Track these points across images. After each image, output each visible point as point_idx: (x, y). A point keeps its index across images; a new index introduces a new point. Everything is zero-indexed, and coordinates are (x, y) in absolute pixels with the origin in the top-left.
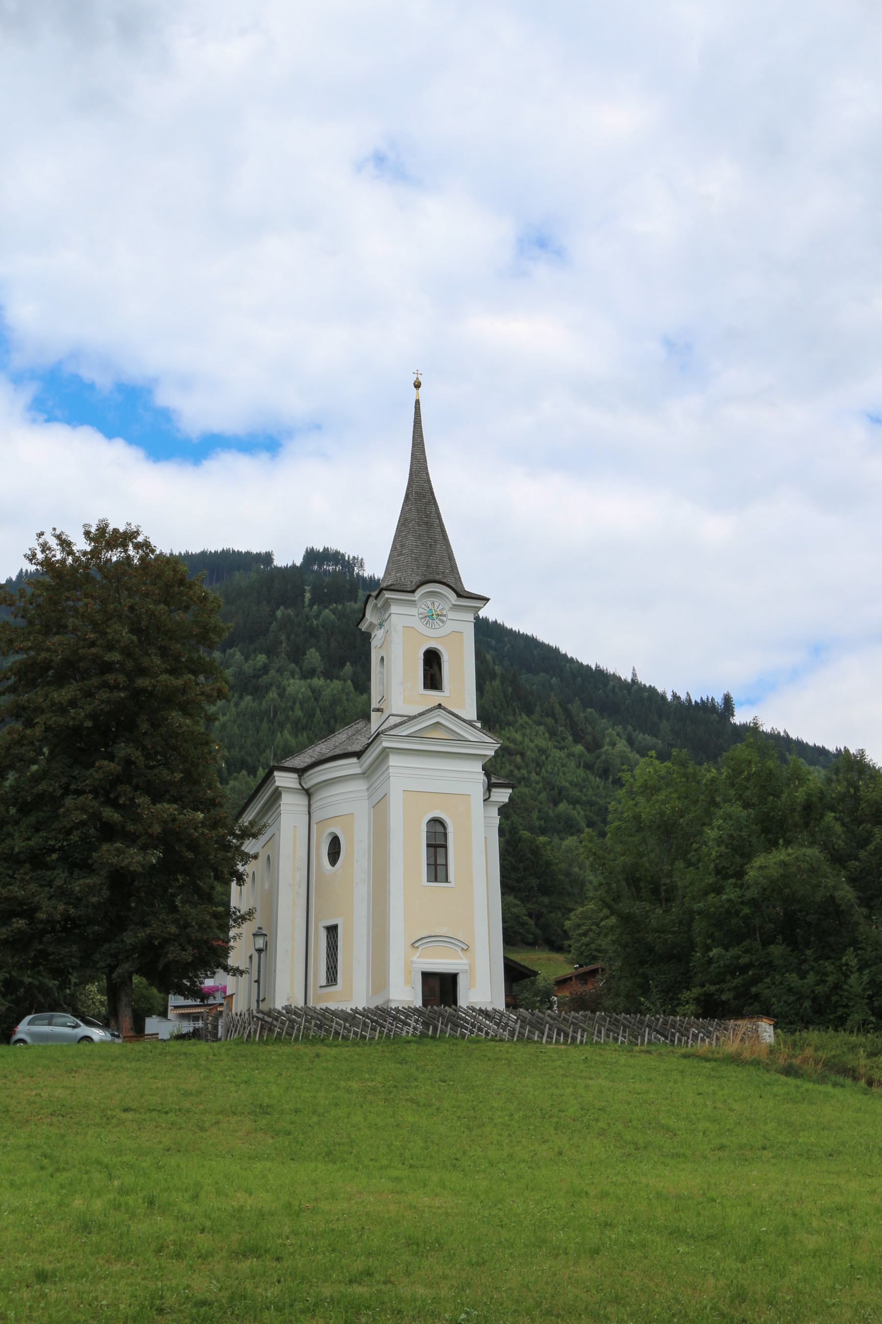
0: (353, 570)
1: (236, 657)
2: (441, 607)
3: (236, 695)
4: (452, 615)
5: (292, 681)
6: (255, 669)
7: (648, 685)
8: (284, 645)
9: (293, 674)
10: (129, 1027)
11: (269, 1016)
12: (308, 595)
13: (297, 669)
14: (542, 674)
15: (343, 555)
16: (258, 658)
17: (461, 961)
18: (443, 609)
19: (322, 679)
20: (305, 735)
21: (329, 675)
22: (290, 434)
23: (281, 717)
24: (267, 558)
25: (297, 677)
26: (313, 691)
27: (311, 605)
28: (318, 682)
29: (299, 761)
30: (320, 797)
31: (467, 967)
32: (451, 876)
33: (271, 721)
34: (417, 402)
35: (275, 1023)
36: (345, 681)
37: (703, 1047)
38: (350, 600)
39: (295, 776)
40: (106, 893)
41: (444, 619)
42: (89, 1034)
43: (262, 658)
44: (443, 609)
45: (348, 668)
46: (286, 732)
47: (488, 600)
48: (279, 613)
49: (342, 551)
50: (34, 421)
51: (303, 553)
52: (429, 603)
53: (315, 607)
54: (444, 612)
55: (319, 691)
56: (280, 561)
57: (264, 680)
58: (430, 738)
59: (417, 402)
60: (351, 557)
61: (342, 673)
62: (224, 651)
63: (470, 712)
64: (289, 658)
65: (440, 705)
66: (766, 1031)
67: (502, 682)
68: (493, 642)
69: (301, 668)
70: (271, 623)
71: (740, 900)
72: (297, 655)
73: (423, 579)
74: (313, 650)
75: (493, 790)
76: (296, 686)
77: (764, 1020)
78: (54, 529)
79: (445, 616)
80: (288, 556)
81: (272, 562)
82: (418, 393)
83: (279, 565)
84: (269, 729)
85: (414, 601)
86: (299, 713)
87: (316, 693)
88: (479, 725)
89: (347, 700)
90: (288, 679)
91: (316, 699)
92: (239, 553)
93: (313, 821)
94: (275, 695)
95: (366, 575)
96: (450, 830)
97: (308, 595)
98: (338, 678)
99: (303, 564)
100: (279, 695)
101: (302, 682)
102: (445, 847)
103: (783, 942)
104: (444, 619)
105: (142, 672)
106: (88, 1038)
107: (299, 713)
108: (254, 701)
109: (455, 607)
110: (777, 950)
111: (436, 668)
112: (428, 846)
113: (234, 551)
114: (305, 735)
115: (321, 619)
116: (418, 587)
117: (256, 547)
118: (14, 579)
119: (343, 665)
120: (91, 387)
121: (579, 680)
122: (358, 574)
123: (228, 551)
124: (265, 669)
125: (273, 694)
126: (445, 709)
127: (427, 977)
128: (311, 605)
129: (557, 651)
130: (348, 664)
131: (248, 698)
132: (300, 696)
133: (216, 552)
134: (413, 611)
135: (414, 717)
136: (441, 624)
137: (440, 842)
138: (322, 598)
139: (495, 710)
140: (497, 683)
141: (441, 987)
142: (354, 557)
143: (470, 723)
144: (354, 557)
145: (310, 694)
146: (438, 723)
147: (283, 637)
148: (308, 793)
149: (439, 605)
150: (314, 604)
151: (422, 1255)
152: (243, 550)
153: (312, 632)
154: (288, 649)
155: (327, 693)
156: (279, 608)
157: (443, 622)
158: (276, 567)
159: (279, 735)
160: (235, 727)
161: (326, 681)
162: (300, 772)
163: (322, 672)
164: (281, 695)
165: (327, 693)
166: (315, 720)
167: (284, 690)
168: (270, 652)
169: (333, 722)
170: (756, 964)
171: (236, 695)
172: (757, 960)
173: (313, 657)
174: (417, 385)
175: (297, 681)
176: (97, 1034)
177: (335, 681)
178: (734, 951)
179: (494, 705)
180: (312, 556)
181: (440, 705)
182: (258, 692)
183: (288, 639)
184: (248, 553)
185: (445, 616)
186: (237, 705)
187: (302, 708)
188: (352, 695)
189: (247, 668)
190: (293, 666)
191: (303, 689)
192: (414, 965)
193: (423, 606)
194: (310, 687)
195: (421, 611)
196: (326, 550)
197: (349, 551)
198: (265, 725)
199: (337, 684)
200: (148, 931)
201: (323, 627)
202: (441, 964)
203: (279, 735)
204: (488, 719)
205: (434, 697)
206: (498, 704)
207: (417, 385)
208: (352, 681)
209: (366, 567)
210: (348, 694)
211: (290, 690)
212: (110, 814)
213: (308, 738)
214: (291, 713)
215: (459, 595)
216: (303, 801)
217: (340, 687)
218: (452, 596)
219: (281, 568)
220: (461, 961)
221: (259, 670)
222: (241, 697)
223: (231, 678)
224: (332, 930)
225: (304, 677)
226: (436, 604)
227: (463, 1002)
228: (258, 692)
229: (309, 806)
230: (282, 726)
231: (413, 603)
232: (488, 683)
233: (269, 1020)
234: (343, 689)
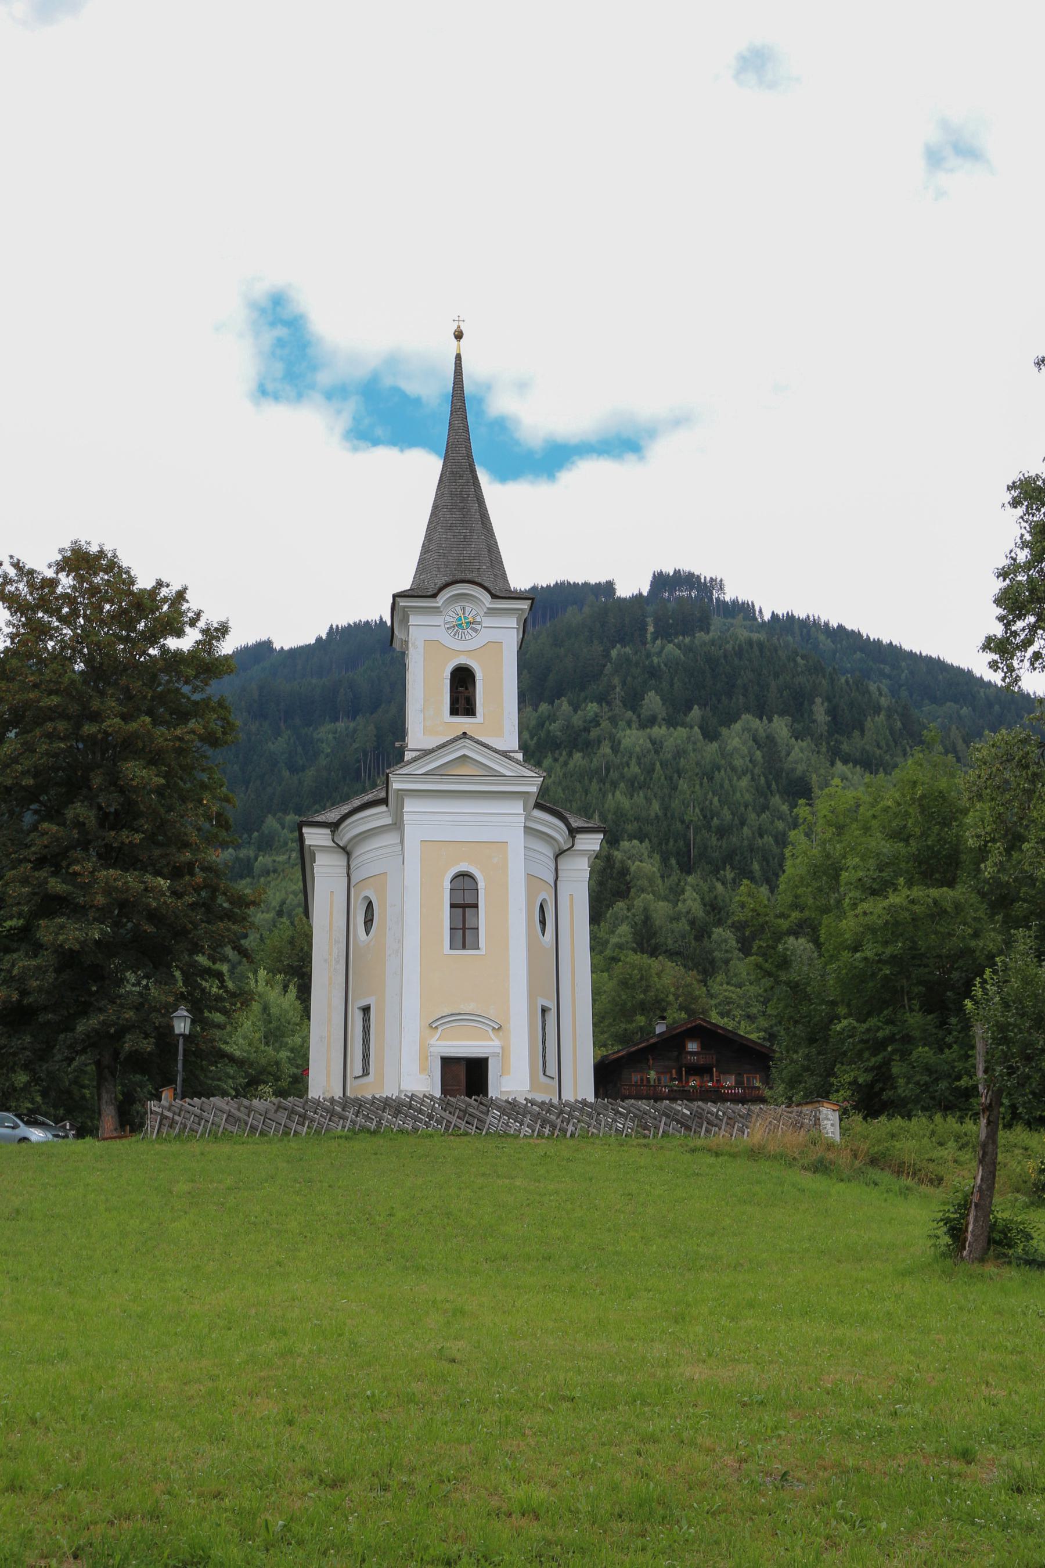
0: (712, 594)
1: (563, 708)
2: (474, 612)
3: (564, 753)
4: (487, 622)
5: (628, 732)
6: (585, 721)
8: (618, 690)
9: (629, 724)
10: (112, 1127)
11: (169, 1110)
12: (651, 629)
13: (634, 718)
14: (948, 704)
15: (699, 577)
16: (588, 708)
18: (477, 615)
19: (664, 728)
20: (641, 794)
21: (672, 722)
22: (652, 433)
23: (614, 775)
24: (608, 587)
25: (634, 726)
26: (653, 743)
27: (655, 639)
28: (658, 731)
29: (333, 815)
30: (364, 853)
31: (499, 1050)
33: (602, 781)
34: (458, 357)
35: (177, 1118)
36: (691, 727)
37: (720, 1137)
38: (701, 630)
39: (327, 831)
40: (51, 976)
41: (478, 627)
42: (27, 1135)
43: (592, 708)
44: (477, 615)
45: (696, 712)
46: (618, 793)
48: (614, 653)
49: (696, 573)
50: (355, 449)
51: (650, 578)
52: (458, 609)
53: (658, 642)
54: (478, 619)
55: (661, 742)
56: (624, 590)
57: (594, 733)
58: (462, 778)
59: (458, 357)
60: (708, 579)
61: (688, 719)
62: (552, 703)
63: (509, 739)
64: (625, 705)
65: (465, 733)
66: (829, 1119)
67: (889, 717)
68: (887, 669)
69: (639, 716)
70: (605, 666)
71: (877, 958)
72: (633, 701)
73: (446, 579)
74: (652, 694)
75: (578, 836)
76: (633, 738)
77: (825, 1105)
78: (11, 557)
79: (479, 623)
80: (632, 584)
81: (615, 593)
82: (459, 346)
83: (623, 595)
84: (600, 789)
85: (438, 608)
86: (635, 769)
87: (657, 745)
88: (520, 756)
89: (694, 750)
90: (624, 730)
91: (657, 752)
92: (576, 585)
93: (352, 885)
94: (608, 751)
95: (727, 599)
96: (481, 885)
97: (651, 629)
98: (683, 725)
99: (651, 592)
100: (612, 748)
101: (640, 733)
102: (476, 906)
103: (920, 1010)
104: (478, 627)
105: (95, 717)
106: (25, 1139)
107: (635, 769)
108: (583, 758)
109: (491, 612)
110: (915, 1020)
111: (470, 689)
112: (452, 906)
113: (569, 583)
114: (641, 794)
115: (663, 655)
116: (441, 589)
117: (595, 577)
118: (324, 638)
119: (691, 709)
120: (417, 401)
121: (997, 708)
122: (718, 599)
123: (563, 583)
124: (595, 722)
125: (606, 749)
126: (471, 738)
127: (447, 1062)
128: (655, 639)
130: (696, 707)
131: (578, 756)
132: (638, 749)
133: (548, 587)
134: (438, 620)
135: (432, 751)
136: (474, 634)
137: (469, 901)
138: (665, 632)
139: (878, 752)
140: (881, 718)
141: (468, 1076)
142: (711, 578)
143: (505, 754)
144: (711, 578)
145: (649, 745)
146: (464, 755)
147: (616, 681)
148: (346, 851)
149: (471, 611)
150: (656, 639)
152: (580, 581)
153: (653, 673)
154: (622, 693)
155: (669, 744)
156: (614, 647)
157: (476, 630)
158: (619, 598)
159: (610, 796)
160: (560, 790)
161: (668, 728)
162: (334, 826)
163: (664, 719)
164: (615, 748)
165: (669, 744)
166: (655, 776)
167: (619, 742)
168: (602, 699)
169: (676, 776)
170: (897, 1037)
171: (564, 753)
172: (899, 1032)
173: (652, 701)
174: (459, 335)
175: (635, 731)
176: (36, 1135)
177: (679, 728)
178: (872, 1022)
179: (879, 746)
180: (660, 581)
181: (465, 733)
182: (589, 747)
183: (624, 683)
184: (586, 584)
185: (479, 623)
186: (566, 764)
187: (639, 764)
188: (698, 744)
189: (577, 720)
190: (630, 713)
191: (641, 741)
192: (432, 1049)
193: (451, 613)
194: (650, 738)
195: (448, 619)
196: (677, 572)
197: (705, 571)
198: (594, 786)
199: (681, 732)
200: (102, 1018)
201: (666, 665)
202: (466, 1046)
203: (610, 796)
204: (536, 747)
205: (463, 723)
206: (883, 743)
207: (459, 335)
208: (700, 728)
209: (727, 589)
210: (695, 743)
211: (626, 742)
212: (56, 886)
213: (646, 798)
214: (626, 769)
215: (494, 596)
216: (340, 860)
217: (685, 735)
218: (485, 598)
219: (625, 599)
221: (590, 722)
222: (570, 755)
223: (559, 733)
224: (366, 1010)
225: (643, 726)
226: (468, 610)
227: (493, 1093)
228: (589, 747)
229: (348, 867)
230: (614, 785)
231: (436, 611)
232: (869, 718)
233: (169, 1114)
234: (689, 738)
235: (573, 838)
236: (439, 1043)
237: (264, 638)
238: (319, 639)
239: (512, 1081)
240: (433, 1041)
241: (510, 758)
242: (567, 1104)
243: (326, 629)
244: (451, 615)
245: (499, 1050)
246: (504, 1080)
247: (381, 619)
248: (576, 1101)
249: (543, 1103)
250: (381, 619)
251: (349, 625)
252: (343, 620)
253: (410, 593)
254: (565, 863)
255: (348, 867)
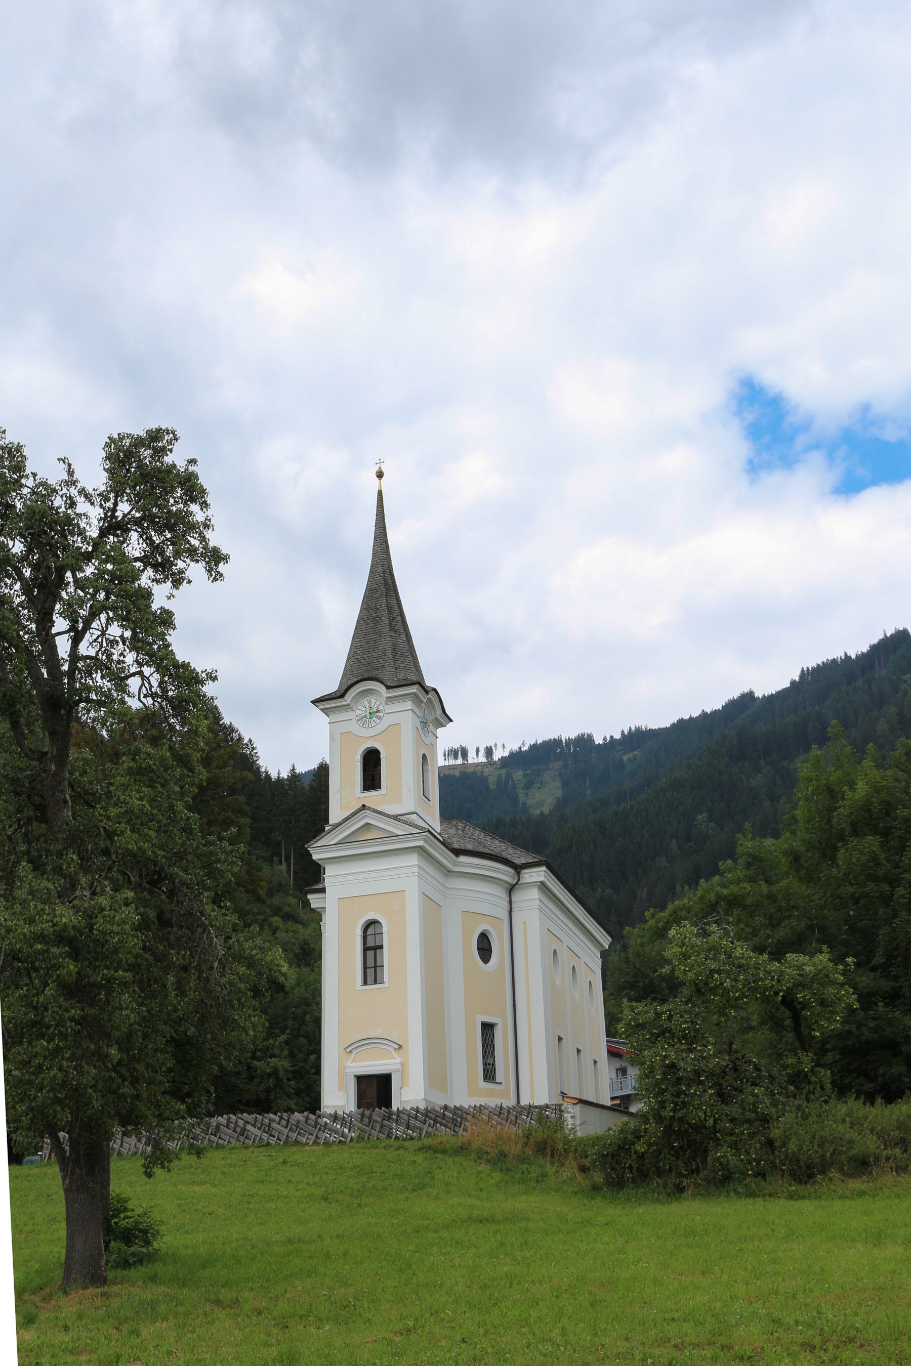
2: (378, 703)
4: (390, 708)
7: (618, 736)
17: (394, 1061)
18: (380, 705)
31: (399, 1067)
32: (386, 978)
34: (380, 493)
41: (381, 714)
44: (380, 705)
47: (451, 721)
52: (366, 702)
54: (381, 708)
59: (380, 493)
65: (364, 806)
73: (367, 675)
75: (524, 871)
79: (382, 711)
85: (421, 702)
109: (390, 700)
129: (681, 721)
134: (350, 715)
136: (378, 721)
146: (367, 824)
149: (375, 702)
151: (715, 1227)
157: (379, 718)
174: (380, 475)
181: (364, 806)
185: (382, 711)
192: (347, 1070)
193: (360, 707)
195: (358, 712)
202: (373, 1066)
207: (380, 475)
220: (394, 1061)
226: (373, 701)
229: (510, 902)
231: (347, 707)
235: (519, 873)
236: (354, 1064)
237: (746, 690)
238: (793, 683)
239: (409, 1094)
240: (348, 1064)
241: (399, 820)
242: (522, 1107)
243: (799, 672)
244: (362, 708)
245: (399, 1067)
246: (403, 1091)
247: (846, 654)
248: (470, 1107)
249: (330, 1115)
250: (846, 654)
251: (818, 665)
252: (812, 662)
253: (334, 696)
254: (517, 897)
255: (510, 902)
